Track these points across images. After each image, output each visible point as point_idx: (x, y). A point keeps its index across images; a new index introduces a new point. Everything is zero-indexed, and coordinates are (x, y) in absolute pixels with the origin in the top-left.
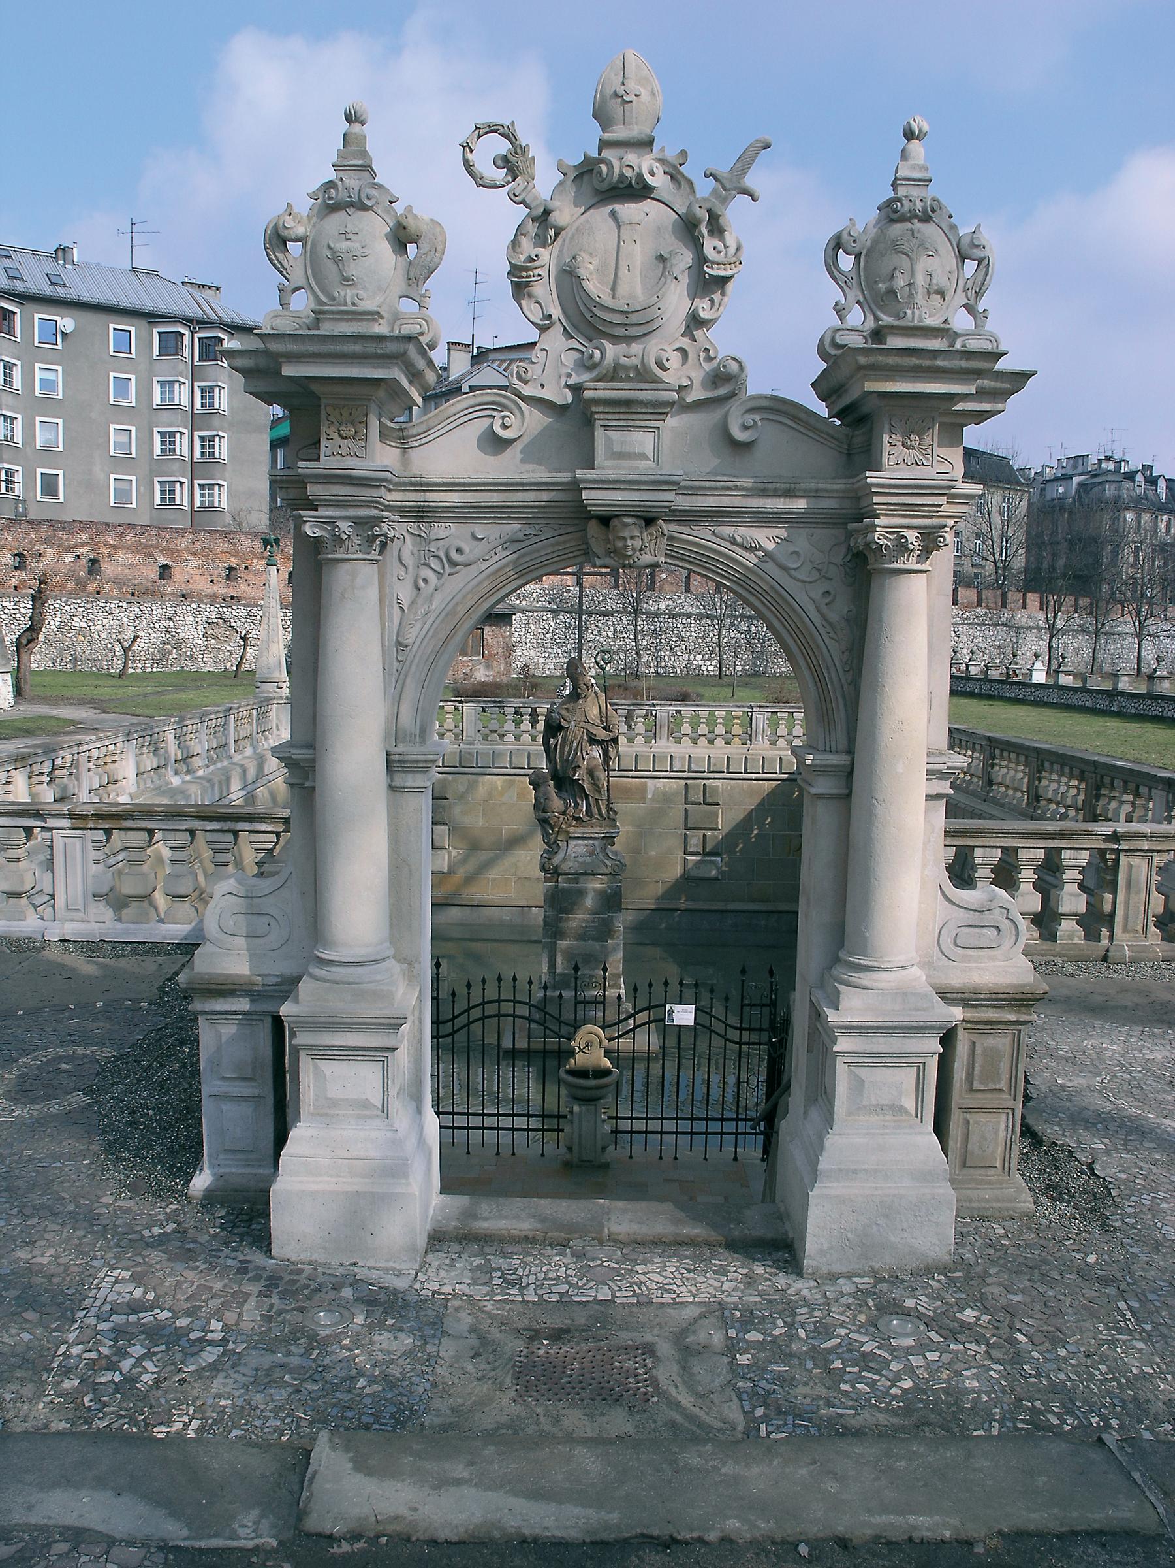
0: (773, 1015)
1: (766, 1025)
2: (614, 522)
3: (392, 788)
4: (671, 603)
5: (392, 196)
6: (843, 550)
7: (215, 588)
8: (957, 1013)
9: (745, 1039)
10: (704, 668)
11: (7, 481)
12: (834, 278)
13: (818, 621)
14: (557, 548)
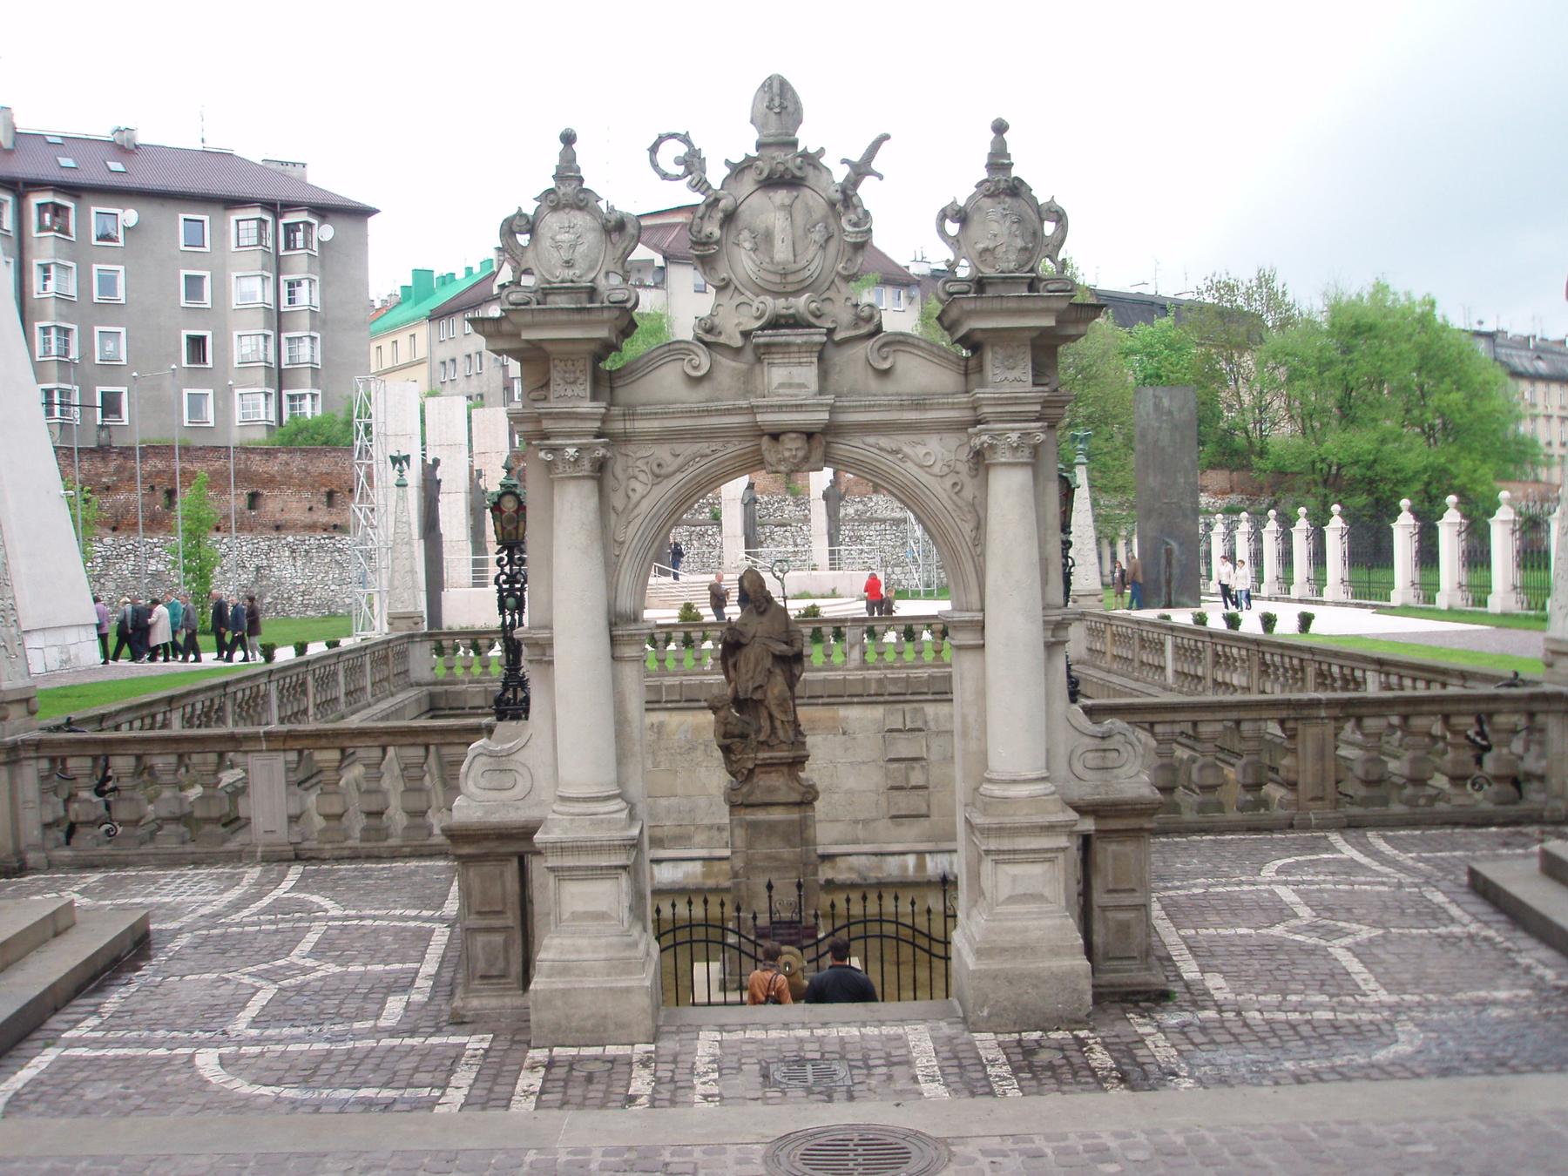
2: (782, 438)
3: (613, 657)
4: (860, 507)
6: (967, 449)
7: (315, 517)
8: (1088, 825)
11: (62, 404)
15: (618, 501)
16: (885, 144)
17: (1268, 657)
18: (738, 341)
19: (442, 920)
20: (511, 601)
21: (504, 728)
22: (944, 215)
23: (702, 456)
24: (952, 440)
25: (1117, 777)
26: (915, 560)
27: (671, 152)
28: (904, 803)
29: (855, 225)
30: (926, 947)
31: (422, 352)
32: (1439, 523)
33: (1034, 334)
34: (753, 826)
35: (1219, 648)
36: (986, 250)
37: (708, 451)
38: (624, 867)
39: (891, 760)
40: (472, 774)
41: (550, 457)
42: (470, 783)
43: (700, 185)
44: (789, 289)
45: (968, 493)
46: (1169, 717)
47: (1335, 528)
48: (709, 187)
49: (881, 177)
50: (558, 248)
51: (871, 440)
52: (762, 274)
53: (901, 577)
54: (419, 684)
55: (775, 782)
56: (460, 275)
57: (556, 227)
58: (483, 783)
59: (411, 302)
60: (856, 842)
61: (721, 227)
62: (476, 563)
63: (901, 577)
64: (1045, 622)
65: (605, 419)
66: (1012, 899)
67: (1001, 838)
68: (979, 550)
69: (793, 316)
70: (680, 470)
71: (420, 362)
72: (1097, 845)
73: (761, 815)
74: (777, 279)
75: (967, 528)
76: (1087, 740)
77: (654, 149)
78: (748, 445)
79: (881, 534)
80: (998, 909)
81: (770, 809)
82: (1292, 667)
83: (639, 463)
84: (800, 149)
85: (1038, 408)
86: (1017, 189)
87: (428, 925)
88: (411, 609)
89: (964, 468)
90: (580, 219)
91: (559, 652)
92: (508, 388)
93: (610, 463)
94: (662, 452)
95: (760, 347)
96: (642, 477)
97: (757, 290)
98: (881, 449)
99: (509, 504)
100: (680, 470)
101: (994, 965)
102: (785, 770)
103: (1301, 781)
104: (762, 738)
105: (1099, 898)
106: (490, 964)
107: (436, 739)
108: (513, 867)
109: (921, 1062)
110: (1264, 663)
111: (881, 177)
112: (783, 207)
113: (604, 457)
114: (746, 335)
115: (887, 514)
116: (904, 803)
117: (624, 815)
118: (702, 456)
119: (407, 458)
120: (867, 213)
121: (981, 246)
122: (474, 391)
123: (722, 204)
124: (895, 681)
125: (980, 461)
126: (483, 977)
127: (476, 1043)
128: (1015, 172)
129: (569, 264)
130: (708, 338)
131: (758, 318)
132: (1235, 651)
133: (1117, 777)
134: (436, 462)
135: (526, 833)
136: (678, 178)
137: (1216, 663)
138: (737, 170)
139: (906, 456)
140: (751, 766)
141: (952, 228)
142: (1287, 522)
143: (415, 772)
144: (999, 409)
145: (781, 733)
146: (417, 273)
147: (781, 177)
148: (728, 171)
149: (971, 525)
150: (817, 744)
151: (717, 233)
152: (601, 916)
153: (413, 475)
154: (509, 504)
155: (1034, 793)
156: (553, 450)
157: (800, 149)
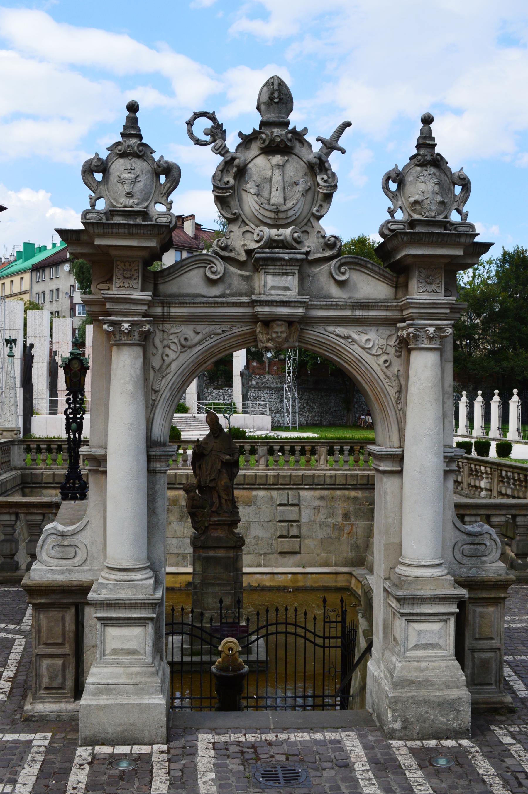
0: (344, 627)
1: (339, 634)
2: (271, 324)
3: (149, 471)
4: (259, 381)
5: (152, 150)
9: (327, 644)
10: (281, 422)
12: (387, 195)
13: (382, 376)
14: (240, 338)
15: (156, 362)
16: (348, 129)
17: (504, 473)
18: (243, 257)
19: (20, 632)
20: (74, 426)
21: (68, 507)
22: (388, 178)
23: (216, 334)
24: (385, 331)
25: (484, 562)
26: (287, 410)
27: (204, 123)
28: (287, 545)
29: (326, 181)
30: (307, 633)
31: (26, 287)
33: (447, 261)
34: (207, 559)
35: (473, 466)
36: (416, 202)
37: (220, 331)
38: (151, 619)
39: (280, 521)
40: (45, 547)
41: (111, 329)
42: (44, 554)
43: (222, 151)
44: (280, 222)
45: (395, 369)
46: (473, 512)
47: (514, 402)
48: (228, 151)
49: (343, 152)
50: (123, 183)
51: (331, 329)
52: (262, 211)
53: (280, 419)
54: (16, 469)
55: (219, 533)
56: (49, 247)
57: (122, 168)
58: (53, 553)
59: (21, 260)
60: (259, 566)
61: (235, 178)
62: (51, 402)
63: (280, 419)
64: (445, 457)
65: (150, 304)
66: (417, 647)
67: (410, 603)
68: (399, 406)
69: (282, 241)
70: (199, 343)
71: (26, 292)
72: (470, 608)
73: (211, 553)
74: (272, 215)
75: (392, 392)
76: (465, 537)
77: (190, 124)
78: (247, 329)
79: (270, 395)
80: (408, 654)
82: (519, 480)
83: (171, 337)
84: (290, 127)
85: (448, 311)
86: (438, 163)
87: (10, 636)
88: (13, 426)
89: (392, 351)
90: (139, 165)
91: (111, 465)
92: (73, 309)
93: (152, 336)
94: (187, 331)
95: (256, 262)
96: (173, 347)
97: (258, 222)
98: (337, 335)
99: (76, 366)
100: (199, 343)
101: (405, 693)
102: (226, 527)
104: (214, 509)
105: (468, 643)
106: (52, 678)
107: (24, 510)
108: (70, 615)
109: (358, 766)
110: (501, 476)
111: (343, 152)
112: (279, 166)
113: (149, 330)
114: (249, 252)
115: (273, 385)
116: (287, 545)
117: (152, 581)
118: (216, 334)
119: (15, 341)
120: (334, 175)
121: (412, 199)
122: (54, 310)
123: (237, 162)
124: (284, 477)
125: (405, 347)
126: (46, 689)
127: (41, 740)
128: (437, 150)
129: (129, 195)
130: (223, 253)
131: (258, 242)
132: (483, 468)
133: (484, 562)
134: (32, 346)
135: (84, 589)
136: (205, 144)
137: (470, 474)
138: (247, 141)
139: (354, 341)
140: (207, 525)
141: (393, 186)
142: (471, 399)
143: (9, 530)
144: (422, 311)
145: (224, 506)
146: (26, 245)
147: (278, 145)
148: (240, 141)
149: (396, 389)
150: (244, 512)
151: (232, 181)
152: (132, 652)
153: (18, 350)
154: (76, 366)
155: (435, 575)
156: (112, 324)
157: (290, 127)
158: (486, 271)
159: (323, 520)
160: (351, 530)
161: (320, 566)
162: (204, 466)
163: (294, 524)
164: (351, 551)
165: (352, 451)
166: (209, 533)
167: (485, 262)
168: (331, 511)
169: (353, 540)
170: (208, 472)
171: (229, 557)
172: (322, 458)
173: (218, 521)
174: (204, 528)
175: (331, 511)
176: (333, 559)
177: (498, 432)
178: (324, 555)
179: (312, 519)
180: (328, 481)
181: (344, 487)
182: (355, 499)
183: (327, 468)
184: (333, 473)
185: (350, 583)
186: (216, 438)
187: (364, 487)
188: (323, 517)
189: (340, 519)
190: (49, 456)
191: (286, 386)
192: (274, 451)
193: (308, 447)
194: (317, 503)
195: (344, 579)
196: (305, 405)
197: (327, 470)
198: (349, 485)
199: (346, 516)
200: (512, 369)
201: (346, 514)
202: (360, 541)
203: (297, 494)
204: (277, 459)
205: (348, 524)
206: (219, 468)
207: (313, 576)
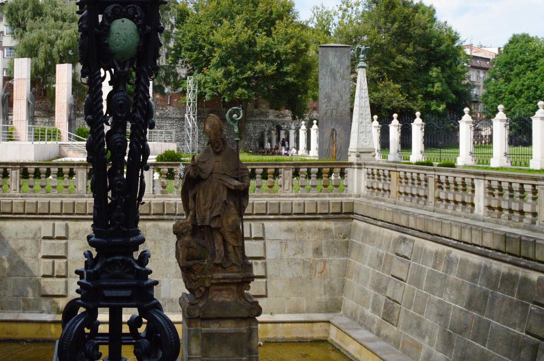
4: (162, 112)
32: (532, 118)
34: (209, 337)
55: (225, 297)
73: (214, 327)
81: (223, 323)
102: (234, 288)
103: (168, 187)
104: (217, 261)
115: (174, 116)
140: (207, 284)
158: (354, 12)
159: (292, 257)
160: (324, 268)
161: (290, 312)
162: (201, 196)
163: (259, 262)
164: (325, 294)
165: (319, 175)
166: (210, 297)
167: (353, 4)
168: (300, 246)
169: (327, 280)
170: (209, 205)
171: (240, 334)
172: (287, 182)
173: (224, 278)
174: (203, 289)
175: (300, 246)
176: (304, 304)
177: (398, 155)
178: (294, 298)
179: (279, 255)
180: (296, 210)
181: (314, 217)
182: (327, 231)
183: (293, 194)
184: (301, 200)
185: (329, 333)
186: (218, 154)
187: (337, 216)
188: (291, 253)
189: (310, 255)
190: (264, 181)
191: (186, 116)
192: (267, 174)
193: (271, 170)
194: (284, 236)
195: (321, 328)
196: (201, 134)
197: (292, 197)
198: (320, 214)
199: (317, 251)
200: (382, 99)
201: (317, 249)
202: (335, 281)
203: (261, 226)
204: (43, 184)
205: (321, 261)
206: (225, 198)
207: (285, 325)
